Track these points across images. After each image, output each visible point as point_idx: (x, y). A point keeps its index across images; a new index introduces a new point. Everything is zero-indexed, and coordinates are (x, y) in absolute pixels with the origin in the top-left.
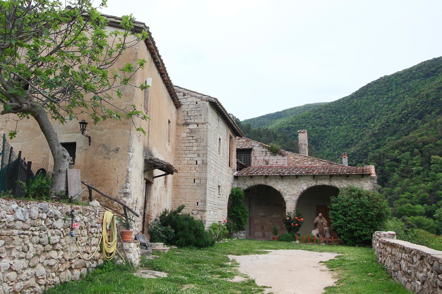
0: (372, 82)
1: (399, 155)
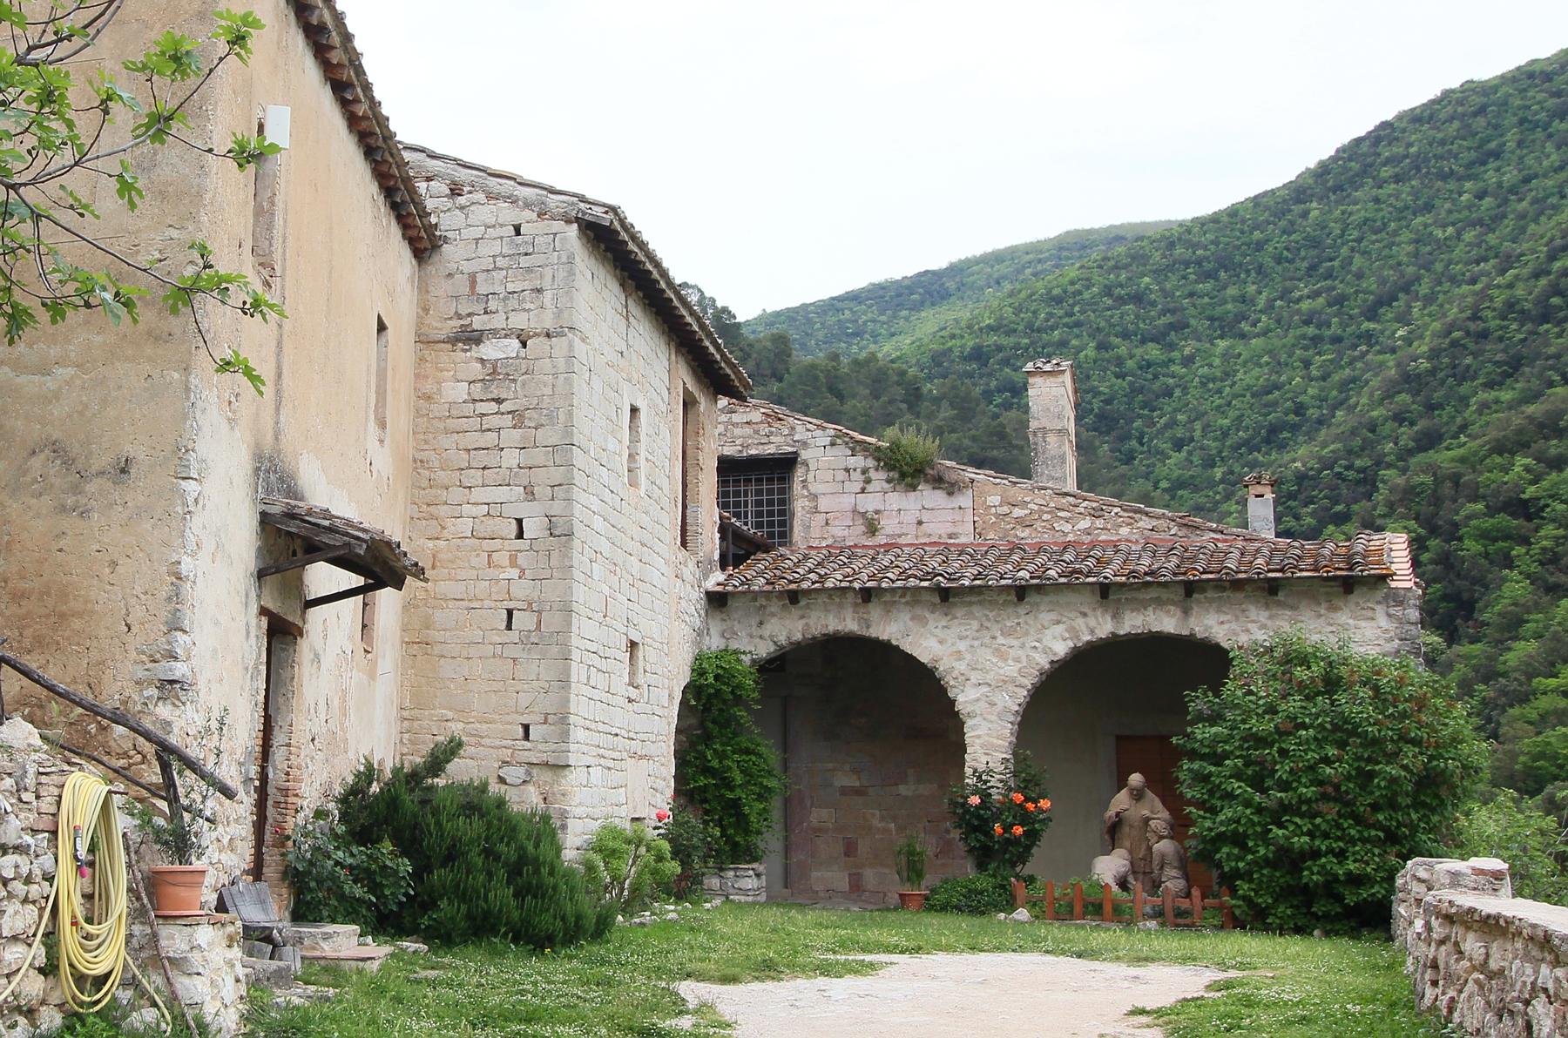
0: (1400, 117)
1: (1533, 482)
